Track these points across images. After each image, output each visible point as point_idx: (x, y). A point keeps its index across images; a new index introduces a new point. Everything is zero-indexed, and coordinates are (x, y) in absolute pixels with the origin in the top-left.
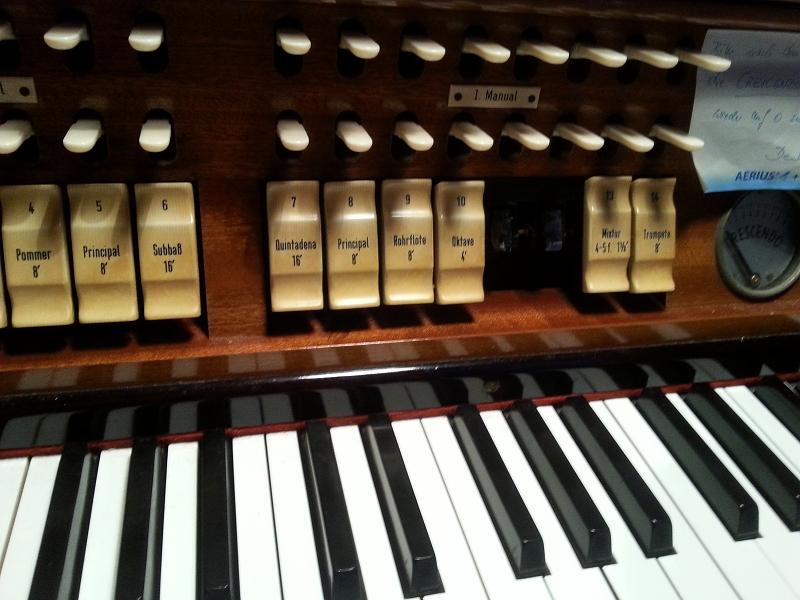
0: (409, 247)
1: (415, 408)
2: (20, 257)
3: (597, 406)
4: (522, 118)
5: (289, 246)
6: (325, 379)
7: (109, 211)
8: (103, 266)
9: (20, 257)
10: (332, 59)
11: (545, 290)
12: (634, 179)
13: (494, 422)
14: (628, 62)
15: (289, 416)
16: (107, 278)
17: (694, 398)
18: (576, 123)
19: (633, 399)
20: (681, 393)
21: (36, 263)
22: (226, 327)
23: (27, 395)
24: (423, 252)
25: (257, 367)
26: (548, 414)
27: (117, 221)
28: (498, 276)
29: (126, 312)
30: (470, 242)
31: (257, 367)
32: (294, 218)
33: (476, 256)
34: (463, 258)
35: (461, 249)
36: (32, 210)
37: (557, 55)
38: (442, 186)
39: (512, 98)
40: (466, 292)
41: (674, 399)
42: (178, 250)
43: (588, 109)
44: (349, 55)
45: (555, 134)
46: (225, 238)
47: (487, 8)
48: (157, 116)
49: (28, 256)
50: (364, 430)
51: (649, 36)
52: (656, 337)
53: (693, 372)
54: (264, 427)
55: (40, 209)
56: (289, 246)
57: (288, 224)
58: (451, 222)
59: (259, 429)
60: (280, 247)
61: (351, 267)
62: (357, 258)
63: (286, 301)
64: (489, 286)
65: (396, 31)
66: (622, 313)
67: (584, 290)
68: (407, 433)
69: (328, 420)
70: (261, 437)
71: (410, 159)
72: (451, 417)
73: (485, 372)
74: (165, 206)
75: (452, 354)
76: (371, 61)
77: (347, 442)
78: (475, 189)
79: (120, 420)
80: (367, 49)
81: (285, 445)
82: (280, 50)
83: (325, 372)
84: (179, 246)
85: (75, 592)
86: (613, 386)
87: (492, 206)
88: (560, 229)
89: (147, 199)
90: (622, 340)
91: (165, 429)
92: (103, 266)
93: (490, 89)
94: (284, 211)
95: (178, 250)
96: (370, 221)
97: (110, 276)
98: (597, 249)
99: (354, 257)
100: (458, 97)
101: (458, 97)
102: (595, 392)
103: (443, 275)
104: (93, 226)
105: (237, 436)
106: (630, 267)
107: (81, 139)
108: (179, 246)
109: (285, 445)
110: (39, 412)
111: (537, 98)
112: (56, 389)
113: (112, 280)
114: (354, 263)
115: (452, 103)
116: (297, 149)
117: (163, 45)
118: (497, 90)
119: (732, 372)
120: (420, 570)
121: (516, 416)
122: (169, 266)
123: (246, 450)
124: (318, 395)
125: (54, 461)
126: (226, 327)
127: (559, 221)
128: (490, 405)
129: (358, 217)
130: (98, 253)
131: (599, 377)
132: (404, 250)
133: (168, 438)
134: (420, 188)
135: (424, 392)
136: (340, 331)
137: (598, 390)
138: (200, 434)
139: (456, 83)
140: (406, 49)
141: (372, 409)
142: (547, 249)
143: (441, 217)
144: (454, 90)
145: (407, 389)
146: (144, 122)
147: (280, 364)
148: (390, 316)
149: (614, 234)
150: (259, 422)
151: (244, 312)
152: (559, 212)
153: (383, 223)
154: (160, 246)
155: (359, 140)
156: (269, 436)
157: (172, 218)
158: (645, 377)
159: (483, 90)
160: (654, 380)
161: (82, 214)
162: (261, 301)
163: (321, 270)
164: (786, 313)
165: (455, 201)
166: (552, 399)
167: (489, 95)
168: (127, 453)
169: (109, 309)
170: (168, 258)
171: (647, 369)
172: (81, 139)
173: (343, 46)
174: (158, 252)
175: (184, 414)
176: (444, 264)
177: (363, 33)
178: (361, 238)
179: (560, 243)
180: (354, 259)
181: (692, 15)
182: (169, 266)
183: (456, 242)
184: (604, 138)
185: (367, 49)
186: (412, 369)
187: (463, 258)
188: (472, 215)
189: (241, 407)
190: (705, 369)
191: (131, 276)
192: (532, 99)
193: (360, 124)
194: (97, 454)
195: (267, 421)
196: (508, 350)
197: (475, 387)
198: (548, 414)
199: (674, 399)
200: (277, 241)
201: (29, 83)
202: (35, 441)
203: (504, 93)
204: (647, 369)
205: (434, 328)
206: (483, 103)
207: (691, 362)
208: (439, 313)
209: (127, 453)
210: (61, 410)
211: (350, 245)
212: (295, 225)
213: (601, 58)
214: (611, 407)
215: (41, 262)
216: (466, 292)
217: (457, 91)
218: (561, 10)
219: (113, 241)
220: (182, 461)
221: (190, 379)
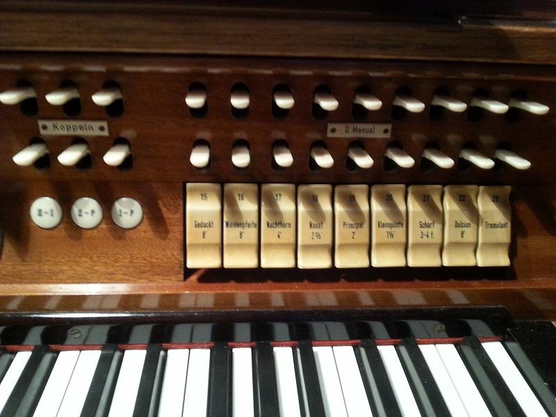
1: (330, 340)
4: (361, 145)
6: (56, 318)
13: (389, 354)
14: (510, 109)
15: (248, 338)
25: (196, 304)
34: (279, 237)
37: (497, 108)
38: (338, 189)
43: (486, 140)
44: (362, 107)
48: (201, 143)
51: (495, 89)
54: (190, 344)
61: (459, 239)
62: (206, 235)
65: (262, 93)
68: (323, 354)
69: (313, 342)
70: (187, 350)
71: (394, 171)
75: (455, 303)
77: (284, 357)
81: (202, 357)
83: (48, 313)
97: (244, 240)
107: (241, 159)
110: (89, 324)
112: (199, 308)
117: (206, 103)
119: (493, 330)
128: (327, 342)
138: (254, 344)
139: (331, 122)
144: (330, 126)
145: (325, 325)
146: (194, 147)
148: (331, 275)
149: (360, 225)
150: (187, 340)
154: (200, 222)
167: (355, 130)
172: (241, 159)
174: (198, 225)
175: (243, 330)
181: (297, 69)
186: (129, 315)
187: (279, 237)
189: (318, 328)
194: (123, 352)
197: (378, 328)
201: (105, 124)
202: (85, 341)
210: (41, 325)
214: (439, 349)
217: (332, 128)
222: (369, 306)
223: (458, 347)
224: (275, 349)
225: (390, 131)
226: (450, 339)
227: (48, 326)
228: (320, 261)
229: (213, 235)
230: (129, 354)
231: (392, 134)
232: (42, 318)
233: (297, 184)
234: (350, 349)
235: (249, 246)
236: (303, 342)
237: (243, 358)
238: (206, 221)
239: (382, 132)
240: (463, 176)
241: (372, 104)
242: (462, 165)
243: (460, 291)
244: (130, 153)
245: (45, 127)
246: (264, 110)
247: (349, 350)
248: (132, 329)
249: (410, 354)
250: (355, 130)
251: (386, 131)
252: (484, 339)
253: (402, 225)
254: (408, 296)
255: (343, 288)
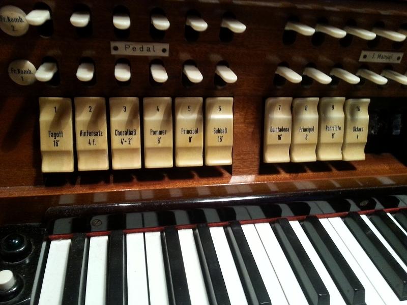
0: (333, 132)
2: (152, 133)
3: (324, 222)
5: (276, 130)
6: (211, 202)
7: (193, 112)
8: (190, 139)
9: (152, 133)
10: (181, 33)
11: (384, 154)
12: (346, 99)
14: (316, 33)
15: (155, 224)
16: (190, 145)
17: (374, 218)
18: (392, 70)
19: (342, 217)
20: (367, 215)
21: (159, 136)
22: (241, 170)
23: (148, 202)
24: (327, 135)
25: (141, 196)
26: (295, 225)
27: (164, 117)
28: (371, 148)
29: (104, 166)
30: (361, 130)
31: (141, 196)
32: (279, 116)
33: (363, 137)
34: (357, 138)
35: (357, 133)
36: (158, 110)
38: (351, 101)
39: (390, 58)
40: (356, 155)
41: (364, 218)
42: (225, 131)
44: (190, 28)
45: (304, 74)
46: (243, 125)
47: (300, 6)
49: (120, 133)
50: (226, 230)
52: (380, 183)
53: (398, 201)
54: (144, 229)
55: (162, 108)
56: (276, 130)
57: (214, 120)
58: (353, 119)
59: (250, 221)
60: (272, 130)
61: (305, 141)
63: (272, 157)
64: (367, 151)
66: (335, 171)
67: (264, 161)
70: (142, 234)
72: (225, 227)
73: (284, 200)
74: (220, 109)
76: (239, 35)
77: (218, 235)
78: (366, 102)
79: (62, 224)
80: (201, 26)
81: (154, 239)
82: (152, 26)
83: (206, 199)
84: (226, 129)
85: (127, 303)
86: (262, 216)
87: (371, 111)
88: (400, 124)
89: (211, 106)
90: (337, 185)
91: (51, 232)
92: (190, 139)
93: (380, 53)
94: (213, 112)
95: (225, 131)
96: (228, 120)
98: (90, 143)
99: (306, 136)
100: (365, 57)
101: (365, 57)
102: (324, 214)
103: (347, 146)
104: (187, 118)
105: (181, 229)
106: (343, 146)
108: (226, 129)
109: (154, 239)
111: (112, 49)
113: (193, 146)
114: (333, 138)
115: (361, 59)
116: (160, 82)
117: (90, 23)
118: (383, 54)
120: (353, 290)
121: (278, 227)
122: (220, 139)
123: (133, 241)
124: (202, 211)
125: (104, 240)
126: (241, 170)
127: (400, 120)
129: (309, 116)
130: (188, 132)
131: (325, 206)
132: (330, 133)
133: (91, 234)
134: (339, 102)
135: (257, 211)
136: (322, 171)
137: (325, 212)
138: (163, 228)
140: (223, 25)
141: (230, 217)
142: (394, 134)
143: (349, 117)
147: (104, 199)
150: (141, 227)
151: (249, 163)
152: (400, 115)
153: (294, 120)
154: (217, 129)
155: (195, 76)
156: (146, 234)
157: (223, 115)
158: (349, 205)
159: (377, 53)
160: (354, 208)
161: (181, 112)
162: (257, 157)
163: (140, 146)
164: (375, 176)
165: (354, 109)
166: (340, 213)
167: (379, 56)
168: (106, 238)
169: (127, 162)
170: (220, 135)
171: (351, 202)
173: (187, 24)
174: (216, 132)
176: (349, 140)
177: (199, 16)
178: (309, 126)
179: (399, 131)
180: (159, 140)
182: (220, 139)
183: (355, 129)
184: (303, 77)
185: (201, 26)
187: (357, 138)
188: (363, 116)
189: (131, 219)
190: (314, 207)
191: (106, 147)
192: (398, 58)
193: (228, 67)
195: (146, 226)
196: (274, 190)
198: (295, 225)
199: (364, 218)
200: (271, 127)
203: (384, 55)
204: (351, 202)
205: (287, 176)
206: (129, 52)
207: (204, 209)
208: (342, 165)
209: (106, 238)
211: (305, 130)
212: (280, 120)
213: (392, 36)
215: (162, 136)
216: (356, 155)
218: (309, 6)
219: (161, 128)
220: (98, 246)
221: (71, 204)
222: (312, 190)
223: (273, 226)
224: (180, 232)
225: (401, 59)
226: (191, 225)
227: (73, 218)
228: (195, 161)
229: (286, 138)
230: (54, 244)
231: (401, 61)
232: (203, 203)
233: (294, 97)
234: (221, 229)
235: (168, 148)
236: (117, 229)
237: (186, 237)
238: (223, 128)
239: (161, 51)
240: (339, 88)
241: (163, 24)
242: (308, 80)
243: (311, 181)
244: (216, 72)
245: (116, 48)
246: (181, 33)
247: (267, 225)
248: (54, 223)
249: (283, 227)
250: (379, 56)
251: (164, 51)
252: (322, 216)
253: (340, 128)
254: (305, 183)
255: (322, 176)
